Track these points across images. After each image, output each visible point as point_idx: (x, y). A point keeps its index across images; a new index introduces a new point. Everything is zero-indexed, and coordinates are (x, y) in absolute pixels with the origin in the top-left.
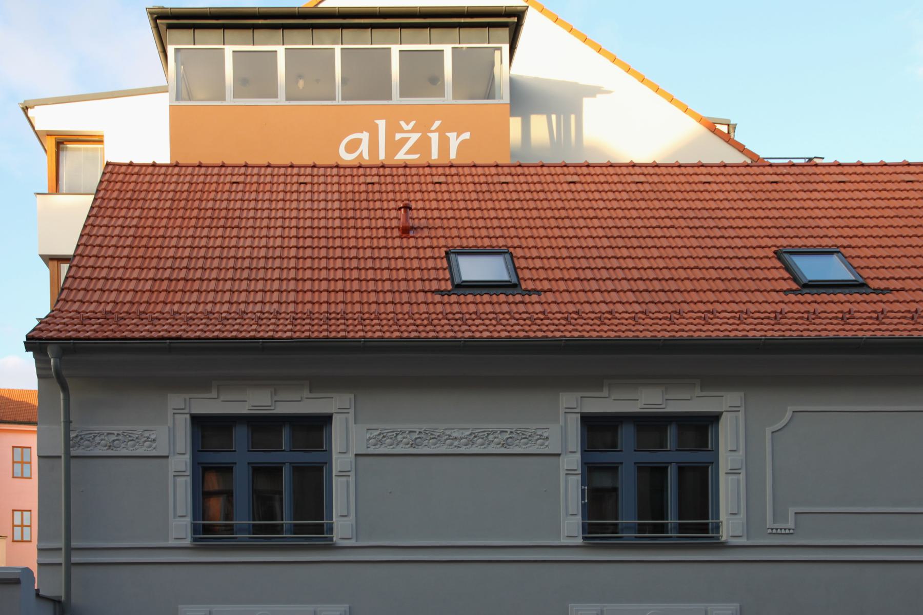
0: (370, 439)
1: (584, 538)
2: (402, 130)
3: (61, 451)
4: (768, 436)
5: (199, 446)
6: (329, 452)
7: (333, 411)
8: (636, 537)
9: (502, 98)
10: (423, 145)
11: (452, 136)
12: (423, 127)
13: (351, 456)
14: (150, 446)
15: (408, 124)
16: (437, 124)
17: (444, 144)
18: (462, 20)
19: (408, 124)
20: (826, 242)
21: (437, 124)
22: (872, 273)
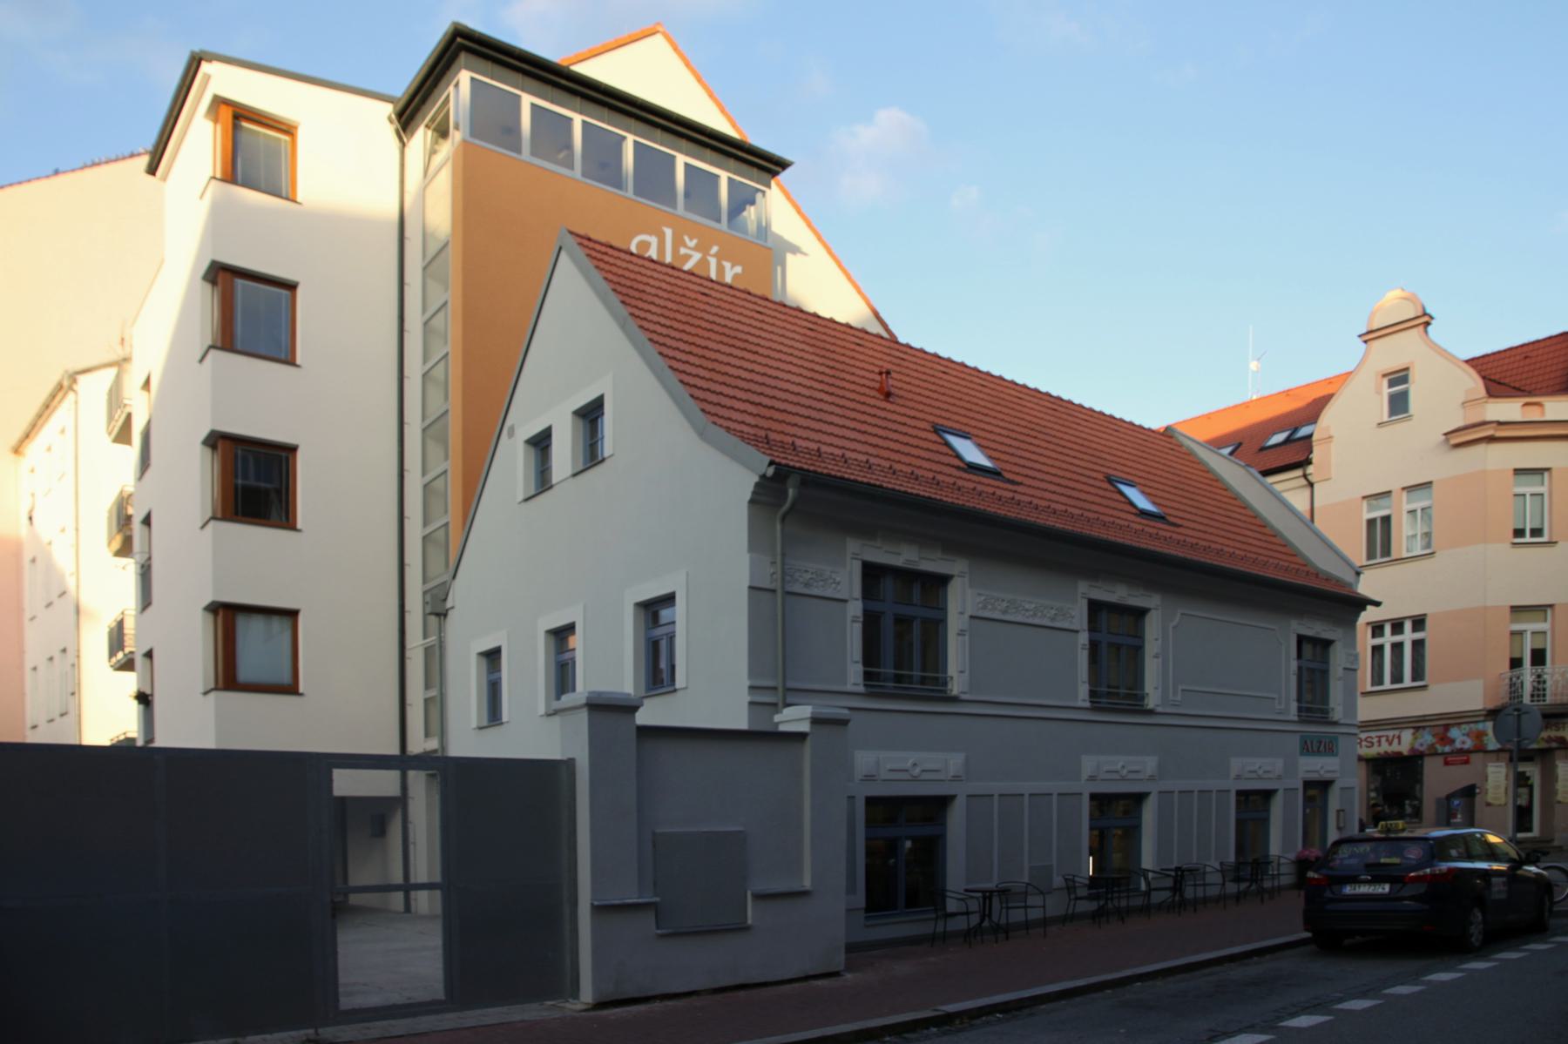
0: (979, 603)
1: (865, 685)
2: (685, 246)
3: (777, 585)
4: (1171, 629)
5: (869, 592)
6: (944, 610)
7: (1152, 607)
8: (895, 687)
9: (627, 191)
10: (703, 262)
11: (727, 265)
12: (703, 248)
13: (966, 616)
14: (835, 589)
15: (691, 239)
16: (715, 249)
17: (721, 270)
18: (740, 153)
19: (691, 239)
20: (964, 428)
21: (715, 249)
22: (1008, 467)
